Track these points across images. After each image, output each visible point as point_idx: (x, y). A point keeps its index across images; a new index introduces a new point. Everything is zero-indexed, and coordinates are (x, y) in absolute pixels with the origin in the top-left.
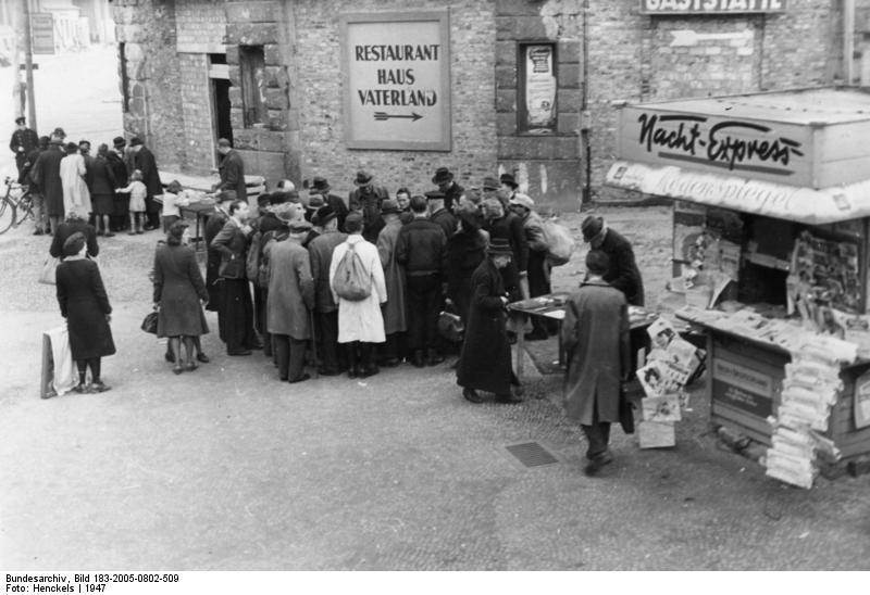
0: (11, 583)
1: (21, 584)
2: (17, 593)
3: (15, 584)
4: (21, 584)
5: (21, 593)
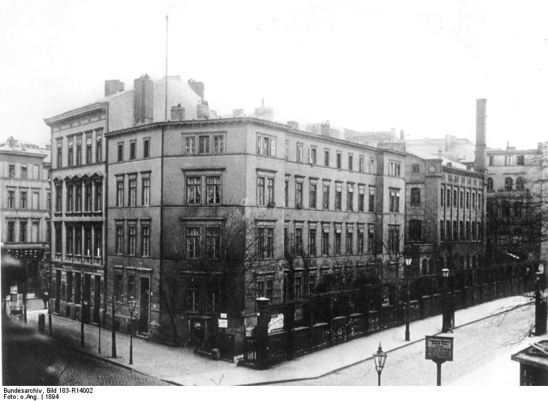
0: (7, 393)
1: (13, 394)
2: (10, 400)
3: (10, 394)
4: (13, 394)
5: (13, 400)
